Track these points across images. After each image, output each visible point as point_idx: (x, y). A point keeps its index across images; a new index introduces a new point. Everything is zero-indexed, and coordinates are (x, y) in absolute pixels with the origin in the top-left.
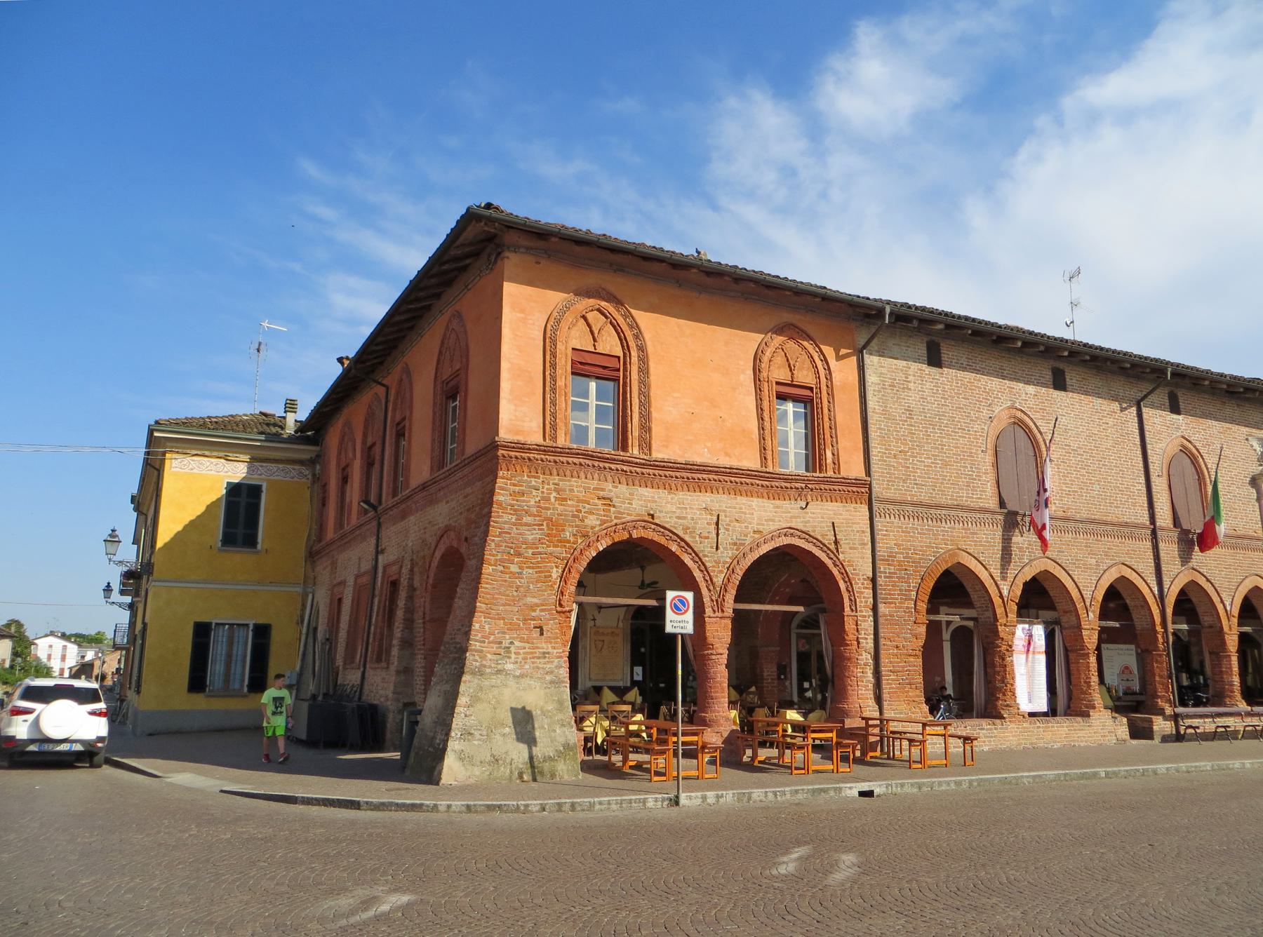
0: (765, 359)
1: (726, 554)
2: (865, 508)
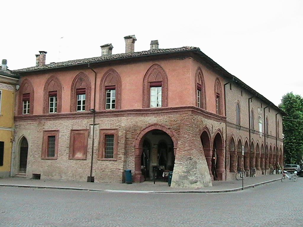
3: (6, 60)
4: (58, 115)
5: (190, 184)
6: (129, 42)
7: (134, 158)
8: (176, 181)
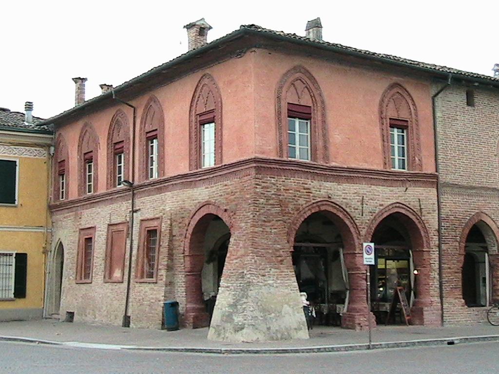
0: (385, 105)
1: (367, 217)
2: (435, 190)
3: (32, 103)
4: (94, 197)
5: (234, 334)
7: (184, 276)
8: (217, 326)
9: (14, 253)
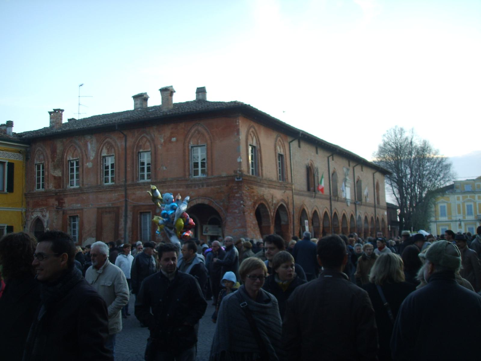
6: (166, 95)
9: (6, 225)
